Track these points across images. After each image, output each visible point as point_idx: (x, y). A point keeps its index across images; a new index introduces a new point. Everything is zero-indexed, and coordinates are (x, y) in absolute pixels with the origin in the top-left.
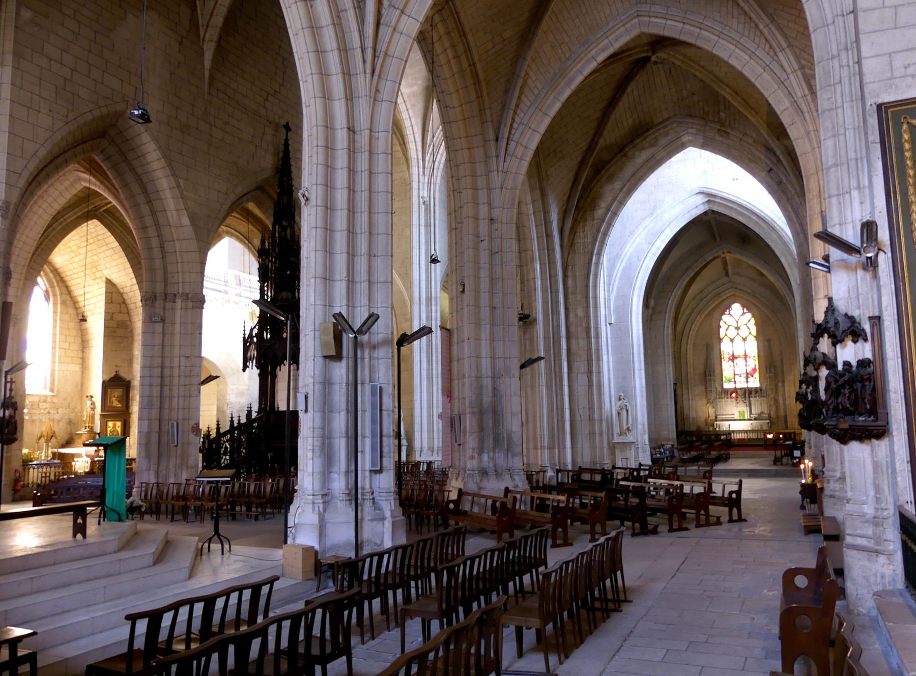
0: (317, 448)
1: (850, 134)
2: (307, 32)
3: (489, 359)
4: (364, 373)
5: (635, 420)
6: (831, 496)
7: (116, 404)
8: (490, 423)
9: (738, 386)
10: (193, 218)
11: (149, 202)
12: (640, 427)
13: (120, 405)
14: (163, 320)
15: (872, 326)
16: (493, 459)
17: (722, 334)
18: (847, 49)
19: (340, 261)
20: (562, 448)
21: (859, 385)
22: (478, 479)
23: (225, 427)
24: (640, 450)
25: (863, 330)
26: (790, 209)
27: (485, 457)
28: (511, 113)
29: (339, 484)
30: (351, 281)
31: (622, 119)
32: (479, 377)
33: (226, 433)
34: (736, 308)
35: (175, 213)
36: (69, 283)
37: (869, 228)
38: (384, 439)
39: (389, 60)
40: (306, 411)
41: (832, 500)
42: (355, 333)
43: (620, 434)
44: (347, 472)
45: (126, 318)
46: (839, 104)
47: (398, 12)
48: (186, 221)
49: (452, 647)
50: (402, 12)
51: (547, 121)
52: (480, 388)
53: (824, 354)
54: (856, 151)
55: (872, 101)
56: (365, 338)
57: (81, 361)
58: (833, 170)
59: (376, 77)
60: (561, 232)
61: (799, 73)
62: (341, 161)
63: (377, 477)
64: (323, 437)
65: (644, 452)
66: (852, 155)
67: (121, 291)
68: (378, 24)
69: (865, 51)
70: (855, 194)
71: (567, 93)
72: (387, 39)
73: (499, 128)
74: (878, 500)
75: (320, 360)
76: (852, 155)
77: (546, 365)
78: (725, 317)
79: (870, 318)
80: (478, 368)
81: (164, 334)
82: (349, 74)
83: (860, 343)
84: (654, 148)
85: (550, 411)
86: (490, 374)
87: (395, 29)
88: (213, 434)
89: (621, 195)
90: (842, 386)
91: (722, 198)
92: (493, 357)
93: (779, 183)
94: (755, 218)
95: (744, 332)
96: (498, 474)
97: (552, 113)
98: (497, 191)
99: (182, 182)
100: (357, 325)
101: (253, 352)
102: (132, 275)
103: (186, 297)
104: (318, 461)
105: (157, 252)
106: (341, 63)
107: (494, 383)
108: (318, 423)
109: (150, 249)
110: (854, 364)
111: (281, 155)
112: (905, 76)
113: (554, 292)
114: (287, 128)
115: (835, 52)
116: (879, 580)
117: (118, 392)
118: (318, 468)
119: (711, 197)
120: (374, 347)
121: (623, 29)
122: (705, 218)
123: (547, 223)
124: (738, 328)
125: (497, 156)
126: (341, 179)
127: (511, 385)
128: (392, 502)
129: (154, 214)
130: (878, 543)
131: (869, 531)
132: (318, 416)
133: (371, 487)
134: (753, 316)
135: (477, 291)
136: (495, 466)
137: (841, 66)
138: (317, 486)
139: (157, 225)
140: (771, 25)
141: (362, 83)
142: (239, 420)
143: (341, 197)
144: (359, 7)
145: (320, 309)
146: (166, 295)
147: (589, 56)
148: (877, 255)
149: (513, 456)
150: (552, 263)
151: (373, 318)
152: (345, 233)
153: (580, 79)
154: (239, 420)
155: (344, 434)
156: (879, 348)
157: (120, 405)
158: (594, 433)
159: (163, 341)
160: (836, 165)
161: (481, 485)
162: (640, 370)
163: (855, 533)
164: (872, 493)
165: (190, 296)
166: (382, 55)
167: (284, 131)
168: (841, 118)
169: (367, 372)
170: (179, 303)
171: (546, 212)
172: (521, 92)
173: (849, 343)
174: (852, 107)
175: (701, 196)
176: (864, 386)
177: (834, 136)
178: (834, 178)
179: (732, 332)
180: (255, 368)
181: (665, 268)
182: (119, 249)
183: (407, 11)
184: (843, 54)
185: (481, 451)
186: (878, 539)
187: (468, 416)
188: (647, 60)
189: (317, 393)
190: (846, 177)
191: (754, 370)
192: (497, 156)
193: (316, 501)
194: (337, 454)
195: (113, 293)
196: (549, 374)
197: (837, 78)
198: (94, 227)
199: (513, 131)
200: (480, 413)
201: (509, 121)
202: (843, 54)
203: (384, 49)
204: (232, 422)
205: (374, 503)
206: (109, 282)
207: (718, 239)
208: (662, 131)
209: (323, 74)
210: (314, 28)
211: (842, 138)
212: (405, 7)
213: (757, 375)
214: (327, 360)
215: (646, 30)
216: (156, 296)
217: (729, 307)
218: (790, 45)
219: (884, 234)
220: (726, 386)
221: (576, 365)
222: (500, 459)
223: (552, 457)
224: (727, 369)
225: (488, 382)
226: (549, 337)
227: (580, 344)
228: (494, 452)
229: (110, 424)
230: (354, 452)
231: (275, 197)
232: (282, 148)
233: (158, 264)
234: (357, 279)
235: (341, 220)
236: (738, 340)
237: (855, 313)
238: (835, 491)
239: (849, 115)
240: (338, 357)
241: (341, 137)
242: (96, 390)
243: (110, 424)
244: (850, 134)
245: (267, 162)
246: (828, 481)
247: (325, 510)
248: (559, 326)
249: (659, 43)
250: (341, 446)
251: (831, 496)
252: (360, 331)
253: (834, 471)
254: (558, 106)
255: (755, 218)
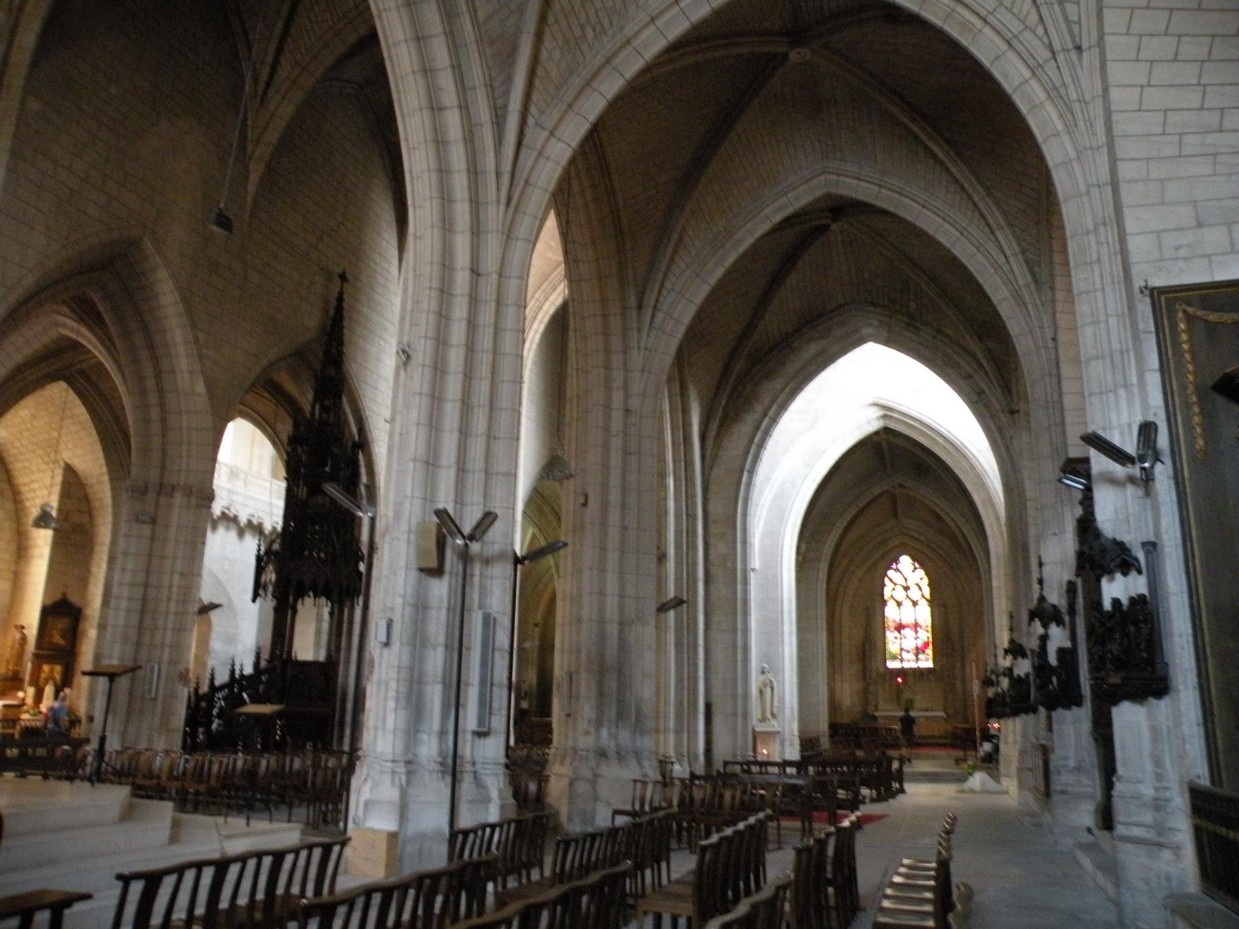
0: (402, 696)
1: (1113, 321)
2: (431, 146)
3: (616, 598)
4: (474, 596)
5: (782, 701)
6: (1063, 792)
7: (58, 640)
8: (614, 688)
9: (906, 665)
10: (210, 385)
11: (155, 359)
12: (787, 711)
13: (62, 642)
14: (154, 521)
15: (1147, 553)
16: (616, 737)
17: (886, 597)
18: (1105, 224)
19: (450, 442)
20: (693, 732)
21: (1132, 628)
22: (593, 763)
23: (222, 678)
24: (787, 744)
25: (1137, 560)
26: (993, 428)
27: (604, 732)
28: (661, 276)
29: (429, 749)
30: (462, 470)
31: (789, 299)
32: (602, 622)
33: (222, 687)
34: (905, 562)
35: (186, 376)
36: (11, 467)
37: (1148, 430)
38: (495, 689)
39: (529, 190)
40: (387, 644)
41: (1065, 797)
42: (464, 537)
43: (763, 719)
44: (442, 733)
45: (86, 519)
46: (1098, 286)
47: (546, 133)
48: (200, 387)
49: (730, 893)
50: (552, 134)
51: (705, 290)
52: (602, 637)
53: (1054, 606)
54: (1120, 342)
55: (1138, 283)
56: (475, 547)
57: (11, 576)
58: (1093, 363)
59: (511, 210)
60: (703, 438)
61: (1020, 257)
62: (460, 310)
63: (482, 742)
64: (411, 681)
65: (792, 745)
66: (1116, 346)
67: (85, 481)
68: (519, 145)
69: (1130, 226)
70: (1122, 392)
71: (733, 257)
72: (529, 164)
73: (643, 293)
74: (1159, 777)
75: (414, 574)
76: (1116, 346)
77: (676, 617)
78: (891, 573)
79: (1144, 544)
80: (602, 610)
81: (153, 539)
82: (477, 203)
83: (1133, 574)
84: (824, 342)
85: (679, 679)
86: (616, 618)
87: (540, 154)
88: (205, 688)
89: (783, 396)
90: (1111, 630)
91: (900, 413)
92: (622, 596)
93: (980, 393)
94: (941, 441)
95: (914, 594)
96: (621, 756)
97: (713, 280)
98: (637, 375)
99: (201, 336)
100: (467, 530)
101: (270, 576)
102: (103, 461)
103: (188, 492)
104: (403, 714)
105: (156, 427)
106: (470, 189)
107: (621, 632)
108: (406, 660)
109: (147, 422)
110: (1125, 601)
111: (332, 312)
112: (1176, 259)
113: (691, 517)
114: (343, 278)
115: (1090, 226)
116: (1164, 883)
117: (61, 624)
118: (401, 725)
119: (887, 411)
120: (487, 562)
121: (805, 186)
122: (876, 439)
123: (687, 425)
124: (906, 589)
125: (639, 330)
126: (458, 333)
127: (644, 634)
128: (501, 778)
129: (158, 375)
130: (1160, 834)
131: (1148, 818)
132: (406, 650)
133: (472, 756)
134: (927, 574)
135: (605, 505)
136: (618, 745)
137: (1099, 243)
138: (400, 747)
139: (161, 391)
140: (987, 199)
141: (494, 215)
142: (241, 671)
143: (456, 358)
144: (498, 124)
145: (418, 503)
146: (161, 485)
147: (763, 214)
148: (1152, 467)
149: (642, 733)
150: (689, 479)
151: (488, 519)
152: (458, 405)
153: (749, 241)
154: (241, 671)
155: (440, 679)
156: (1154, 582)
157: (62, 642)
158: (735, 714)
159: (151, 549)
160: (1097, 358)
161: (599, 772)
162: (791, 633)
163: (1128, 820)
164: (1149, 767)
165: (194, 490)
166: (522, 183)
167: (338, 281)
168: (1101, 304)
169: (476, 596)
170: (178, 498)
171: (686, 412)
172: (675, 252)
173: (1118, 576)
174: (1114, 290)
175: (875, 409)
176: (1138, 629)
177: (1093, 323)
178: (1097, 373)
179: (900, 594)
180: (270, 596)
181: (820, 503)
182: (91, 424)
183: (557, 134)
184: (1102, 229)
185: (599, 723)
186: (1161, 828)
187: (584, 675)
188: (824, 229)
189: (407, 618)
190: (1109, 372)
191: (926, 645)
192: (639, 330)
193: (397, 770)
194: (428, 706)
195: (73, 483)
196: (679, 630)
197: (1095, 257)
198: (59, 391)
199: (662, 299)
200: (601, 673)
201: (658, 285)
202: (1102, 229)
203: (524, 176)
204: (233, 672)
205: (475, 778)
206: (69, 470)
207: (889, 466)
208: (836, 320)
209: (446, 199)
210: (440, 142)
211: (1102, 326)
212: (556, 127)
213: (929, 651)
214: (423, 575)
215: (833, 190)
216: (146, 487)
217: (896, 561)
218: (1010, 225)
219: (1163, 441)
220: (892, 665)
221: (715, 618)
222: (625, 736)
223: (678, 745)
224: (893, 642)
225: (612, 630)
226: (682, 578)
227: (720, 589)
228: (617, 727)
229: (46, 668)
230: (455, 702)
231: (318, 367)
232: (334, 303)
233: (156, 442)
234: (469, 467)
235: (453, 387)
236: (907, 604)
237: (1125, 538)
238: (1067, 785)
239: (1113, 300)
240: (438, 572)
241: (462, 279)
242: (31, 617)
243: (46, 668)
244: (1113, 321)
245: (311, 321)
246: (1059, 772)
247: (408, 782)
248: (695, 564)
249: (840, 208)
250: (435, 696)
251: (1063, 792)
252: (472, 537)
253: (1066, 758)
254: (720, 272)
255: (941, 441)
